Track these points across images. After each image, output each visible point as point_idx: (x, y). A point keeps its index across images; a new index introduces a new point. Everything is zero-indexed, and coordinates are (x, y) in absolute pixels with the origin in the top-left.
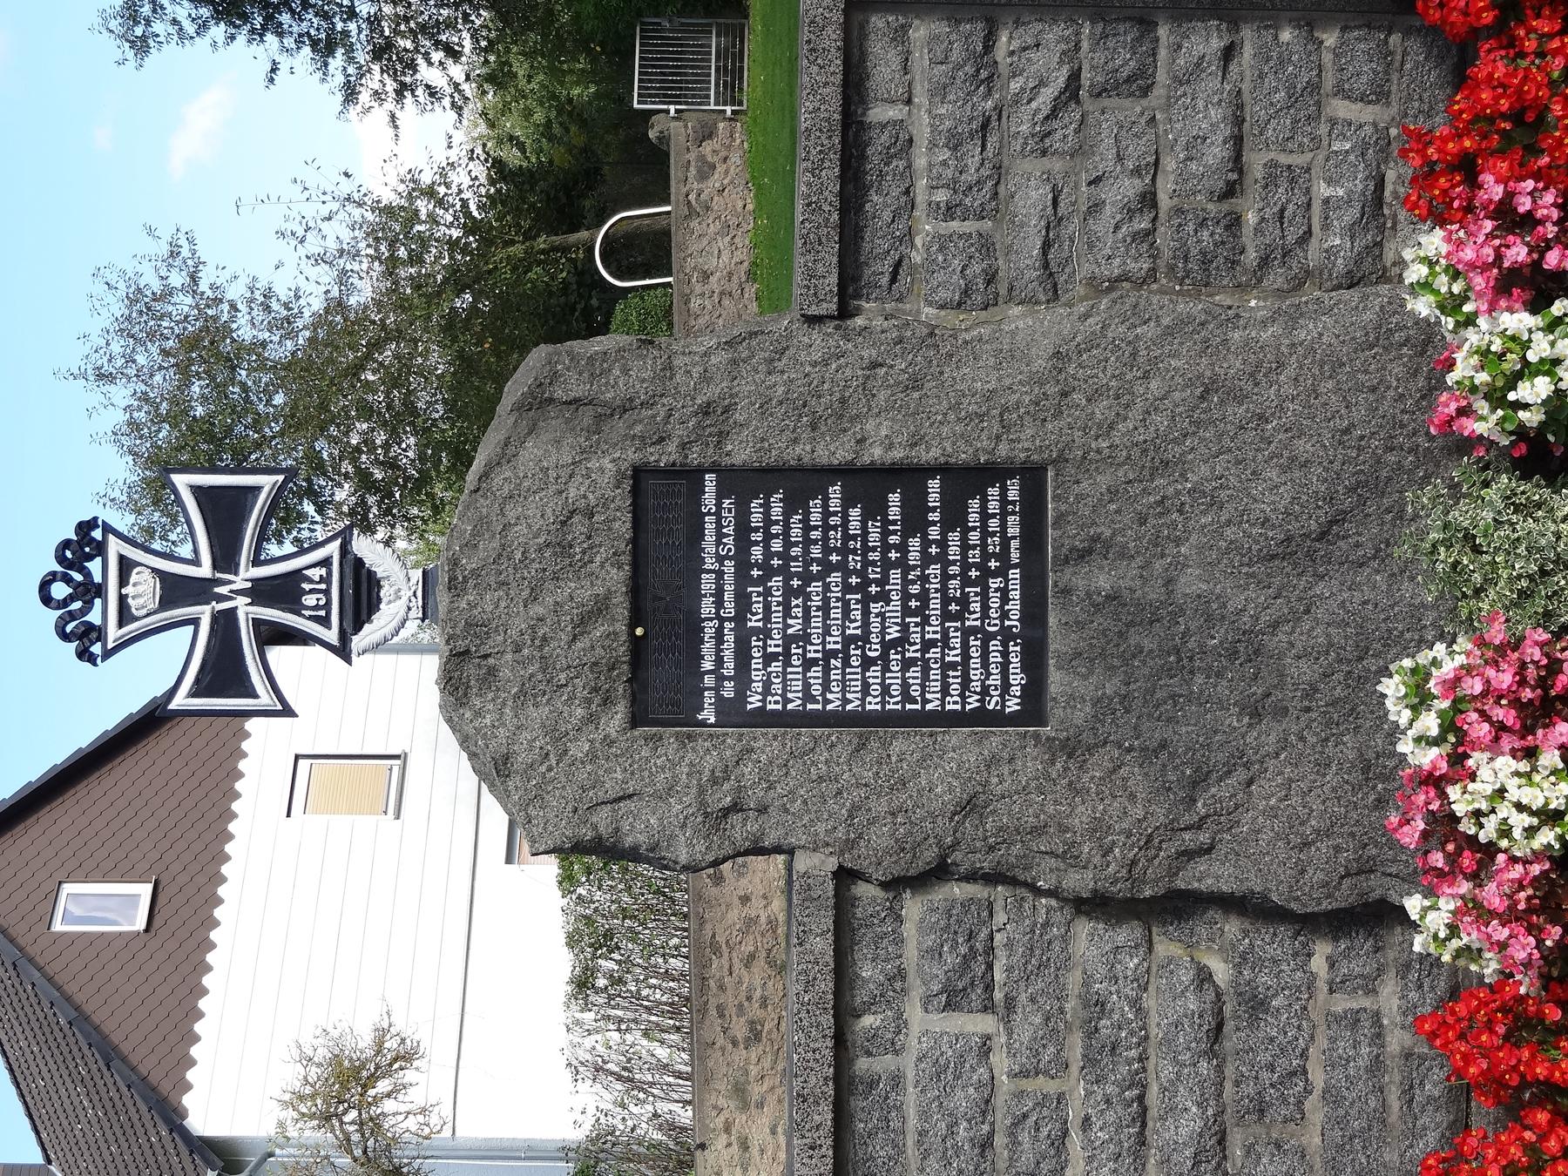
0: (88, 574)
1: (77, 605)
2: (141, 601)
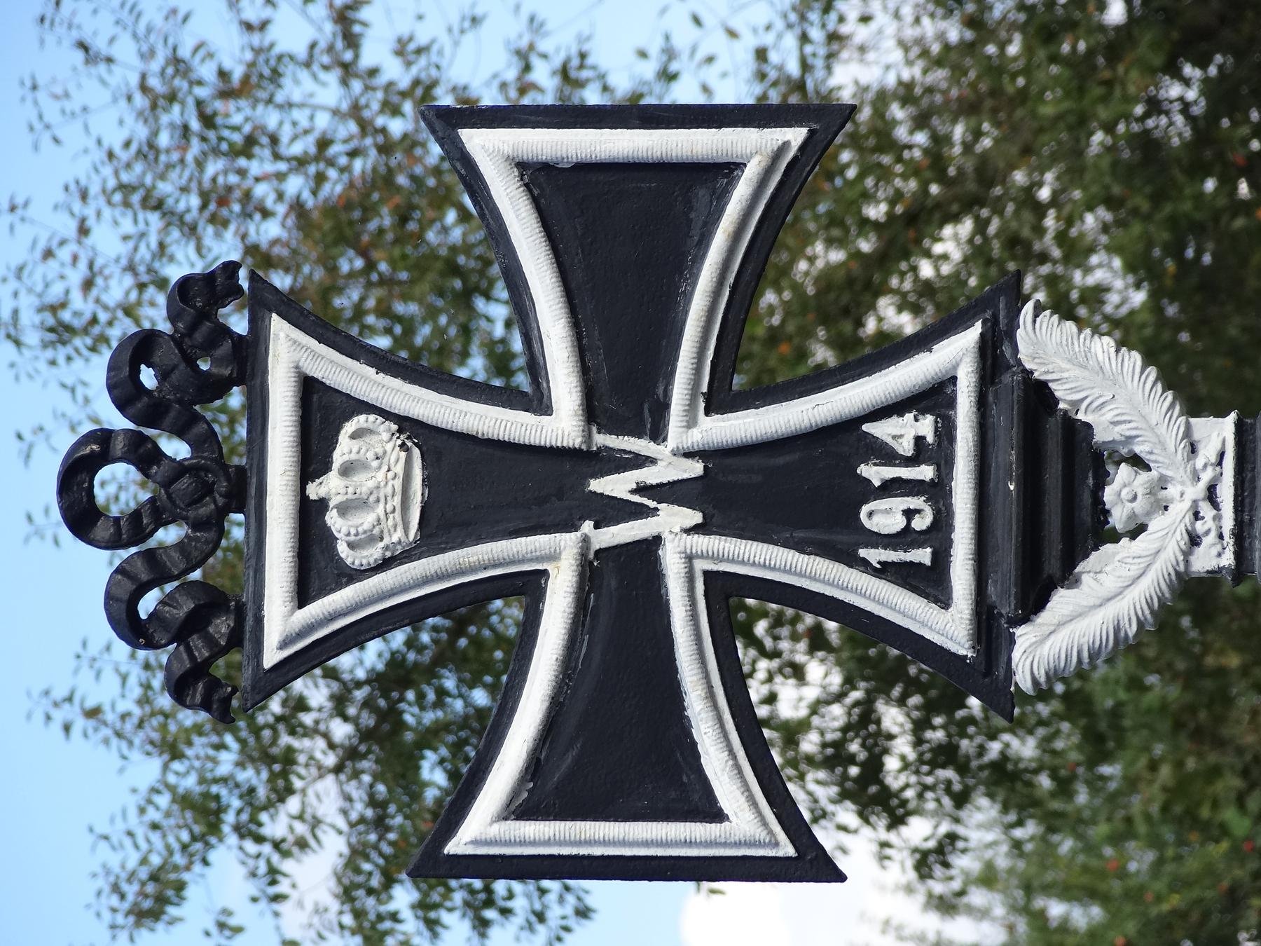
0: (205, 441)
1: (169, 535)
2: (366, 520)
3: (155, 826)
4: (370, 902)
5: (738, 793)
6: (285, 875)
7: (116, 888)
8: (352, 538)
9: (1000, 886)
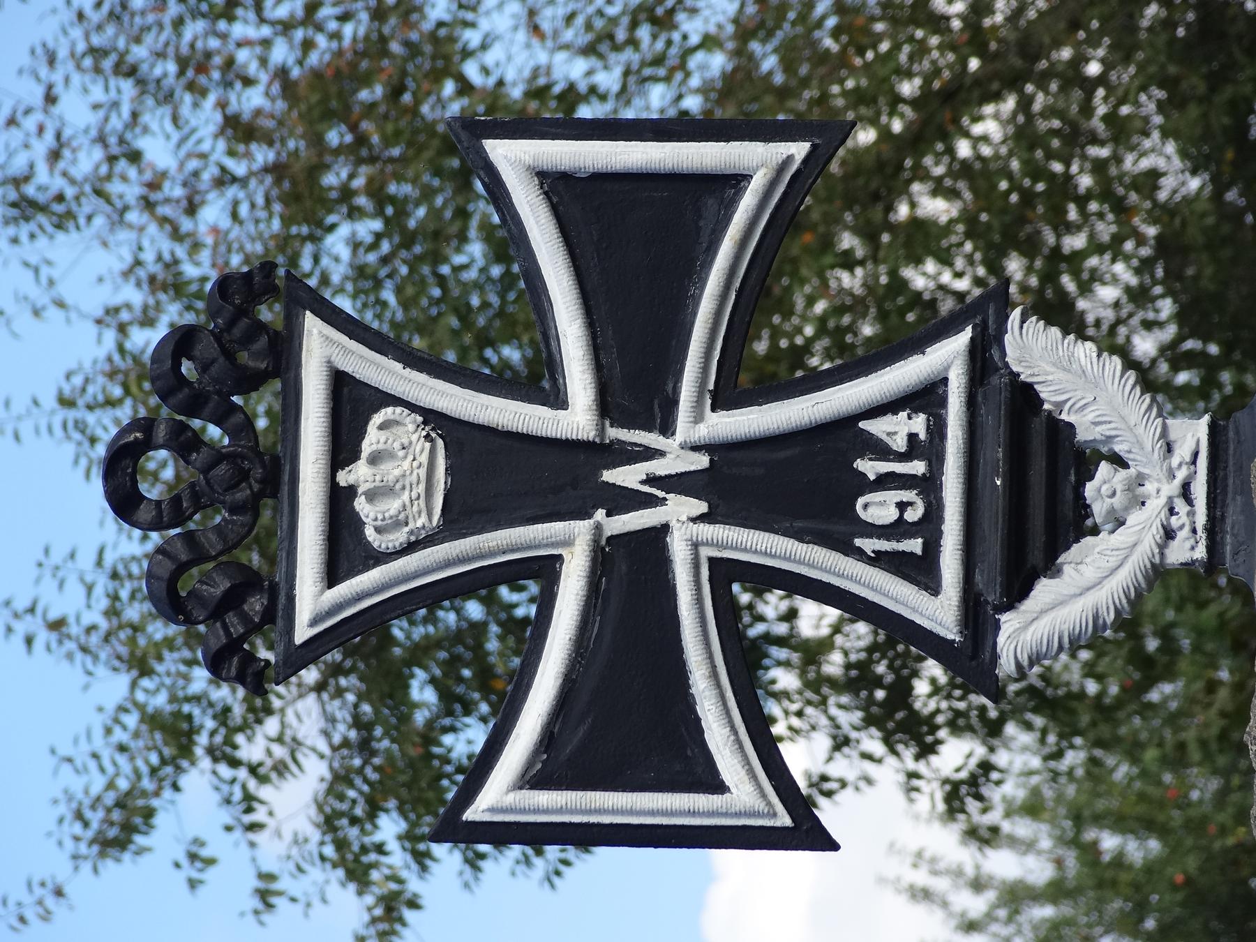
0: (242, 427)
2: (392, 506)
3: (122, 748)
4: (353, 832)
5: (739, 767)
6: (262, 802)
7: (79, 816)
8: (379, 523)
9: (1046, 815)
